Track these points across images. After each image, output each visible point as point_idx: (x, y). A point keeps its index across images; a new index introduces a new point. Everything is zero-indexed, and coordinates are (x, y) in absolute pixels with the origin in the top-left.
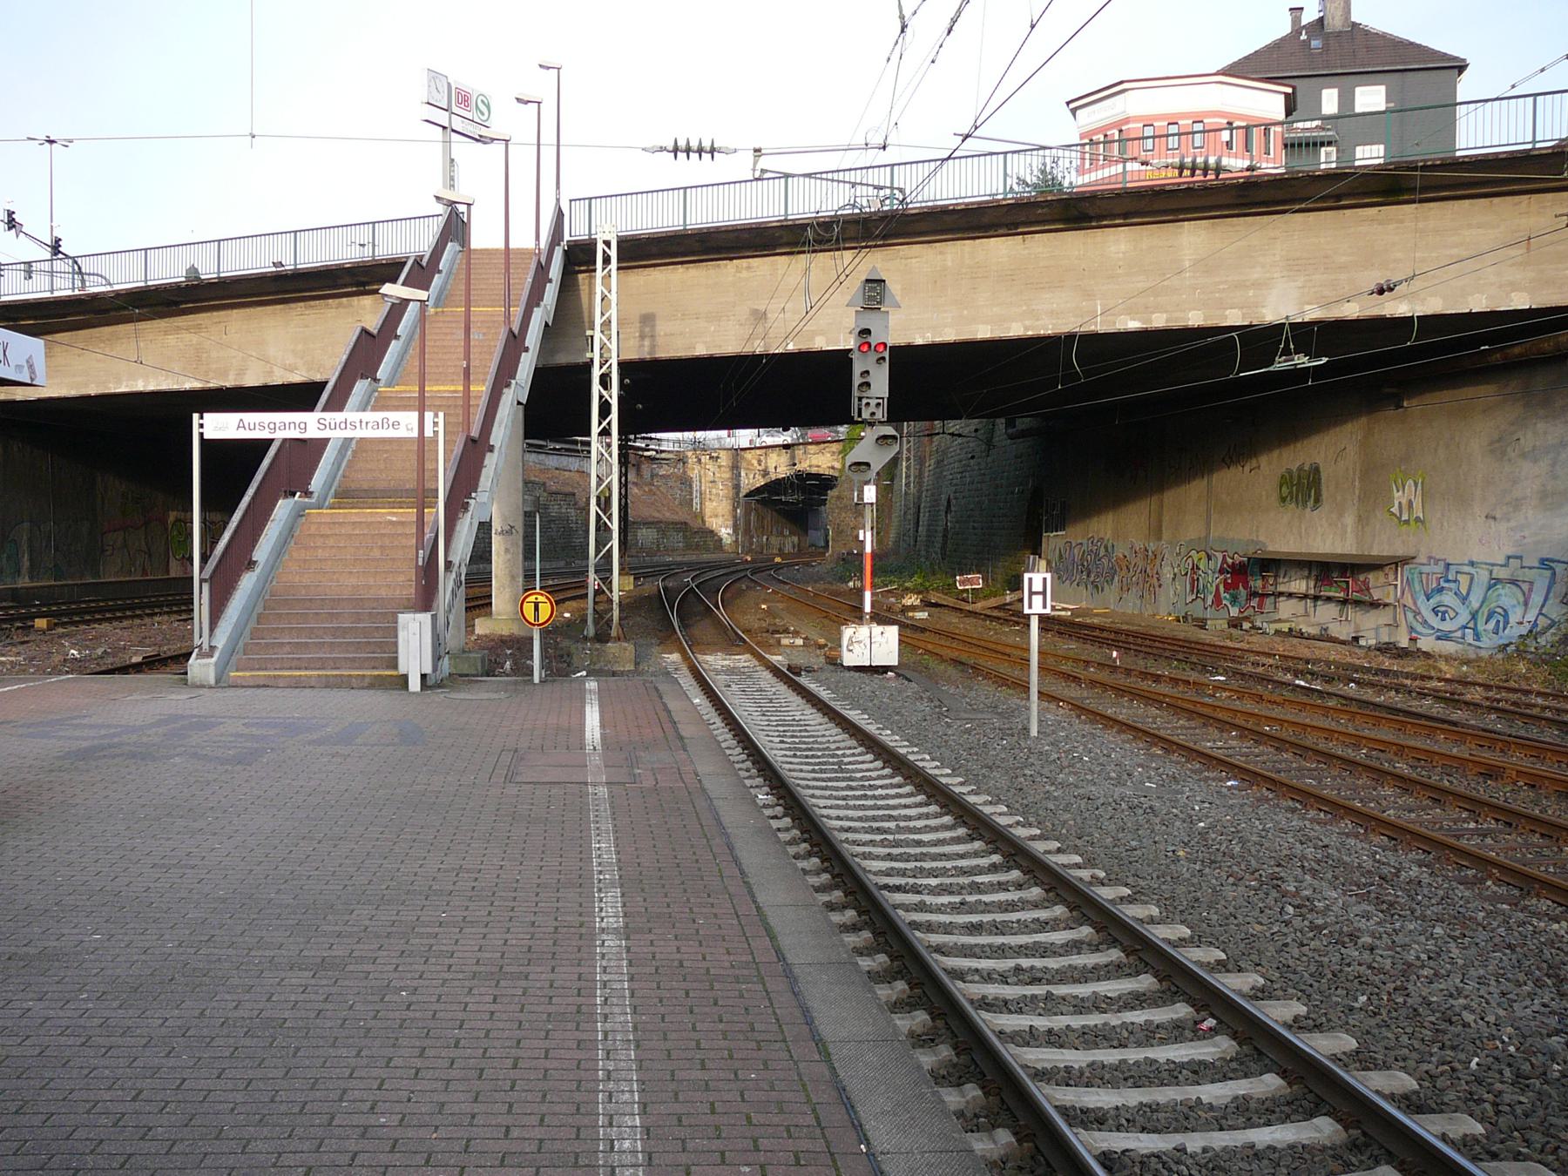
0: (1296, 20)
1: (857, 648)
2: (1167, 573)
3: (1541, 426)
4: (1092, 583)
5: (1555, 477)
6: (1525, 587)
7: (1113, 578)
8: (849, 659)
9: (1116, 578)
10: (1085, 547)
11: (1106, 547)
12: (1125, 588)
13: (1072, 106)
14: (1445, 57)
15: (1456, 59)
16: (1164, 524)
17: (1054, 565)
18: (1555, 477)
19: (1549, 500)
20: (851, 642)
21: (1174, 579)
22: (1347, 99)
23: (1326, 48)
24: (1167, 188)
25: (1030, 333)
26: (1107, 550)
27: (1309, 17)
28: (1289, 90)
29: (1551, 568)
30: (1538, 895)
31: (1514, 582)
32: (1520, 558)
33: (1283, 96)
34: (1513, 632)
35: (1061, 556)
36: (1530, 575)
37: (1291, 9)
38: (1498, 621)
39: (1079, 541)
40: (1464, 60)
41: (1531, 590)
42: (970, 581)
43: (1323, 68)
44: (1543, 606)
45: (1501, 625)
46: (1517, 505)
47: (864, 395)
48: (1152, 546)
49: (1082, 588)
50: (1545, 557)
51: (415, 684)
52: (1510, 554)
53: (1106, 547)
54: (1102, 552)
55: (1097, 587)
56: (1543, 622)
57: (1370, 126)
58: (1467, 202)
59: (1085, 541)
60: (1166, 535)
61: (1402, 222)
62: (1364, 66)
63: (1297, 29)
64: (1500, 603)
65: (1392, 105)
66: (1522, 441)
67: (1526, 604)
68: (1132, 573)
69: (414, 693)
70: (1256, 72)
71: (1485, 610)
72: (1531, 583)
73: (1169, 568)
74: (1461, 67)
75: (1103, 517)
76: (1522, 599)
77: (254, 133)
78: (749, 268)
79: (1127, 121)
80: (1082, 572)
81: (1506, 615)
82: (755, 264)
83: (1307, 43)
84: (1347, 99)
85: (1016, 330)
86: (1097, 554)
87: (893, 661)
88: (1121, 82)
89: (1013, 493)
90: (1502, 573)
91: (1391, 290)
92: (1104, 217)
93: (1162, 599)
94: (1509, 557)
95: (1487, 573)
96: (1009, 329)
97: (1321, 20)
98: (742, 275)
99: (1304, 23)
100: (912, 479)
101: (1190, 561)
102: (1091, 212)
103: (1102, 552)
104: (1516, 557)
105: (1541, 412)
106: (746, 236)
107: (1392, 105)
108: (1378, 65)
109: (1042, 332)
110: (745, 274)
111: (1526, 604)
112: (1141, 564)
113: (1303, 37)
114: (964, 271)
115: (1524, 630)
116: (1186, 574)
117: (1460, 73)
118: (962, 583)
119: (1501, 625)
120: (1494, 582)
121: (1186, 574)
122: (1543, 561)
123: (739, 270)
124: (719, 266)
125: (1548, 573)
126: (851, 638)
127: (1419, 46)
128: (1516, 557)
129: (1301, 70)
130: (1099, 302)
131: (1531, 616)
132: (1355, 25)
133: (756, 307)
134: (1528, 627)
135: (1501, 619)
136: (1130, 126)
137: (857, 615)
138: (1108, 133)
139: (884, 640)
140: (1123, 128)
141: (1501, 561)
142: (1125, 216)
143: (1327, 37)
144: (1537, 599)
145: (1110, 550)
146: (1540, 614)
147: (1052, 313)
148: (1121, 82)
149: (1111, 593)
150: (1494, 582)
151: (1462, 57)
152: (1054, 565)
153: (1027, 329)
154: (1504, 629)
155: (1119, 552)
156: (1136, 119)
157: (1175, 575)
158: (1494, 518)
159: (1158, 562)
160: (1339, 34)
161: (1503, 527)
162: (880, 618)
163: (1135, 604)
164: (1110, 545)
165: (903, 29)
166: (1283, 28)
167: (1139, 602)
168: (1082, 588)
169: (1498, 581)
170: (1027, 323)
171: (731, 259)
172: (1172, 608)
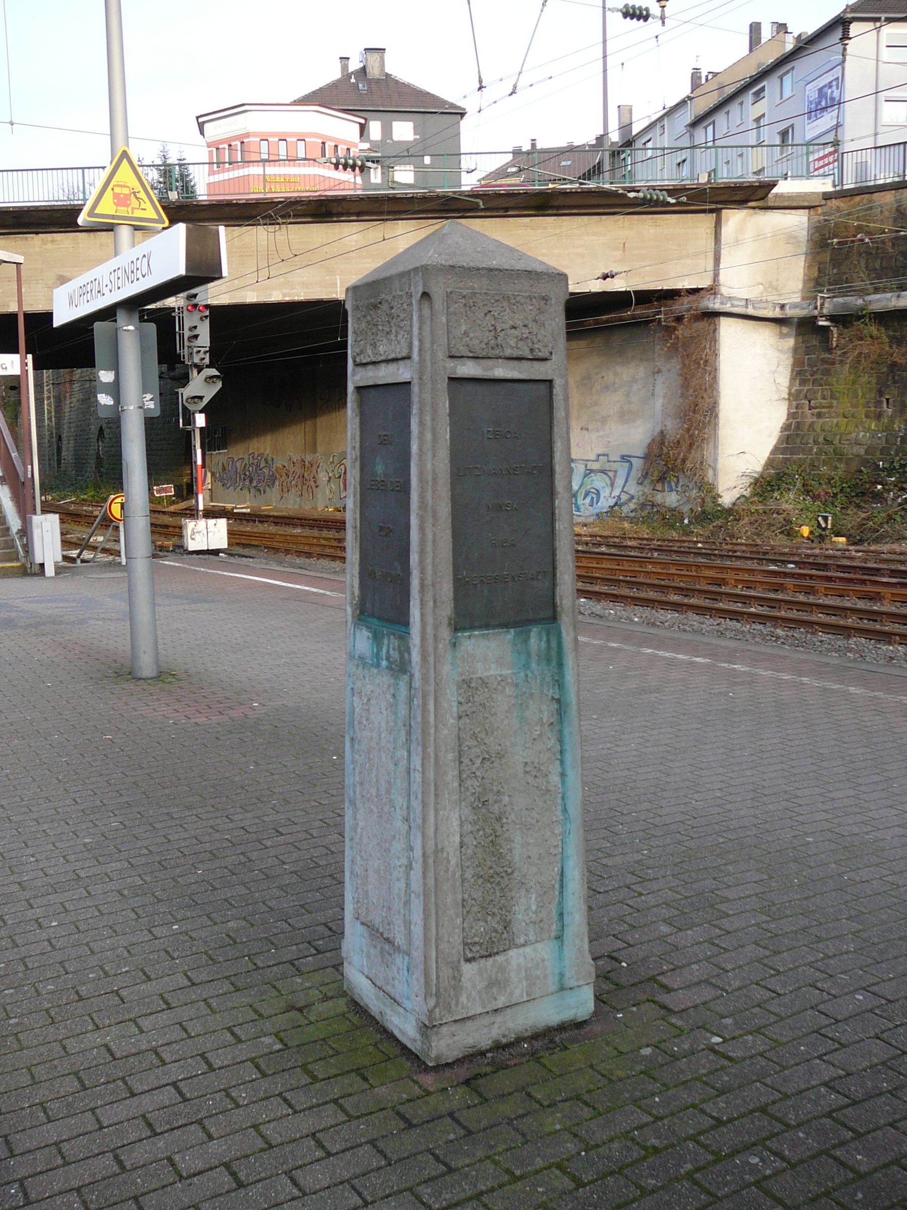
0: (345, 68)
1: (197, 536)
2: (323, 477)
3: (619, 369)
4: (255, 487)
5: (630, 403)
6: (611, 474)
7: (274, 483)
8: (192, 546)
9: (277, 483)
10: (246, 461)
11: (266, 460)
12: (284, 489)
13: (201, 120)
14: (453, 106)
15: (459, 108)
16: (318, 442)
17: (218, 475)
18: (630, 403)
19: (626, 417)
20: (193, 533)
21: (329, 481)
22: (387, 131)
23: (370, 91)
24: (398, 196)
25: (287, 299)
26: (267, 463)
27: (354, 65)
28: (363, 121)
29: (629, 461)
30: (854, 636)
31: (603, 472)
32: (607, 455)
33: (358, 126)
34: (605, 503)
35: (224, 469)
36: (615, 466)
37: (341, 58)
38: (593, 498)
39: (241, 457)
40: (464, 109)
41: (615, 476)
42: (165, 490)
43: (370, 105)
44: (624, 486)
45: (595, 500)
46: (604, 420)
47: (192, 344)
48: (308, 458)
49: (246, 491)
50: (624, 454)
51: (50, 571)
52: (599, 453)
53: (266, 460)
54: (263, 464)
55: (259, 490)
56: (624, 497)
57: (407, 154)
58: (586, 218)
59: (246, 457)
60: (320, 449)
61: (545, 228)
62: (397, 106)
63: (346, 76)
64: (594, 486)
65: (418, 137)
66: (606, 378)
67: (612, 485)
68: (291, 478)
69: (50, 578)
70: (338, 105)
71: (583, 491)
72: (616, 472)
73: (324, 473)
74: (462, 115)
75: (262, 439)
76: (609, 482)
77: (14, 121)
78: (53, 241)
79: (248, 135)
80: (245, 479)
81: (598, 493)
82: (59, 238)
83: (356, 86)
84: (387, 131)
85: (276, 296)
86: (258, 466)
87: (224, 544)
88: (243, 105)
89: (169, 422)
90: (595, 466)
91: (613, 277)
92: (342, 215)
93: (319, 495)
94: (599, 455)
95: (583, 466)
96: (270, 295)
97: (364, 69)
98: (47, 247)
99: (351, 70)
100: (53, 414)
101: (342, 467)
102: (334, 211)
103: (263, 464)
104: (604, 455)
105: (619, 360)
106: (58, 215)
107: (418, 137)
108: (408, 107)
109: (296, 298)
110: (50, 246)
111: (612, 485)
112: (299, 471)
113: (353, 80)
114: (234, 250)
115: (612, 502)
116: (340, 477)
117: (462, 118)
118: (159, 491)
119: (595, 500)
120: (589, 472)
121: (340, 477)
122: (623, 457)
123: (44, 242)
124: (26, 238)
125: (627, 464)
126: (193, 530)
127: (433, 96)
128: (604, 455)
129: (354, 105)
130: (338, 277)
131: (616, 493)
132: (387, 75)
133: (61, 273)
134: (614, 500)
135: (595, 496)
136: (251, 139)
137: (192, 513)
138: (233, 144)
139: (216, 530)
140: (245, 140)
141: (593, 457)
142: (358, 214)
143: (370, 82)
144: (620, 482)
145: (270, 462)
146: (623, 491)
147: (304, 285)
148: (243, 105)
149: (273, 494)
150: (589, 472)
151: (463, 106)
152: (218, 475)
153: (284, 295)
154: (597, 503)
155: (278, 464)
156: (255, 134)
157: (330, 478)
158: (587, 429)
159: (314, 468)
160: (378, 81)
161: (594, 435)
162: (210, 514)
163: (295, 501)
164: (269, 459)
165: (513, 93)
166: (336, 75)
167: (298, 499)
168: (246, 491)
169: (592, 471)
170: (285, 291)
171: (37, 233)
172: (328, 502)
